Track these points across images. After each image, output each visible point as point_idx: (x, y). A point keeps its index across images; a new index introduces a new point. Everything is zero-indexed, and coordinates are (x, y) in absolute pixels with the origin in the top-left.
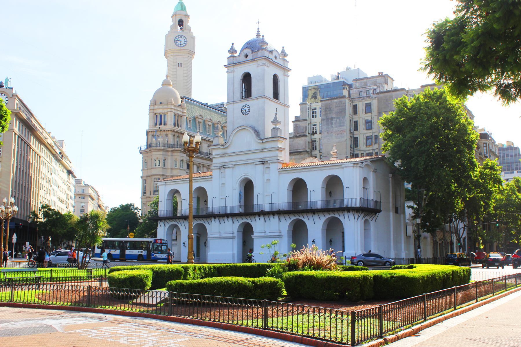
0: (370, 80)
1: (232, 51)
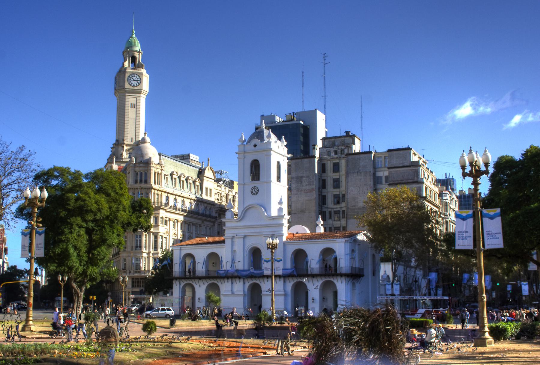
0: (339, 139)
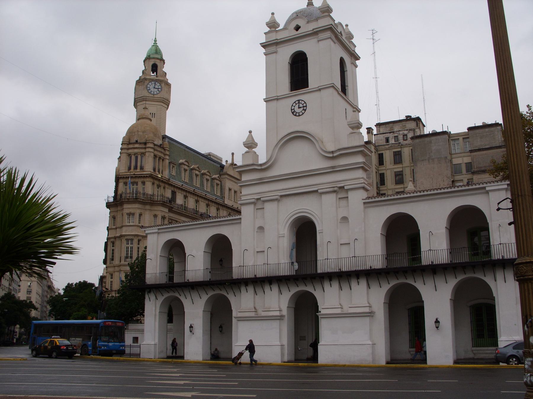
1: (272, 25)
